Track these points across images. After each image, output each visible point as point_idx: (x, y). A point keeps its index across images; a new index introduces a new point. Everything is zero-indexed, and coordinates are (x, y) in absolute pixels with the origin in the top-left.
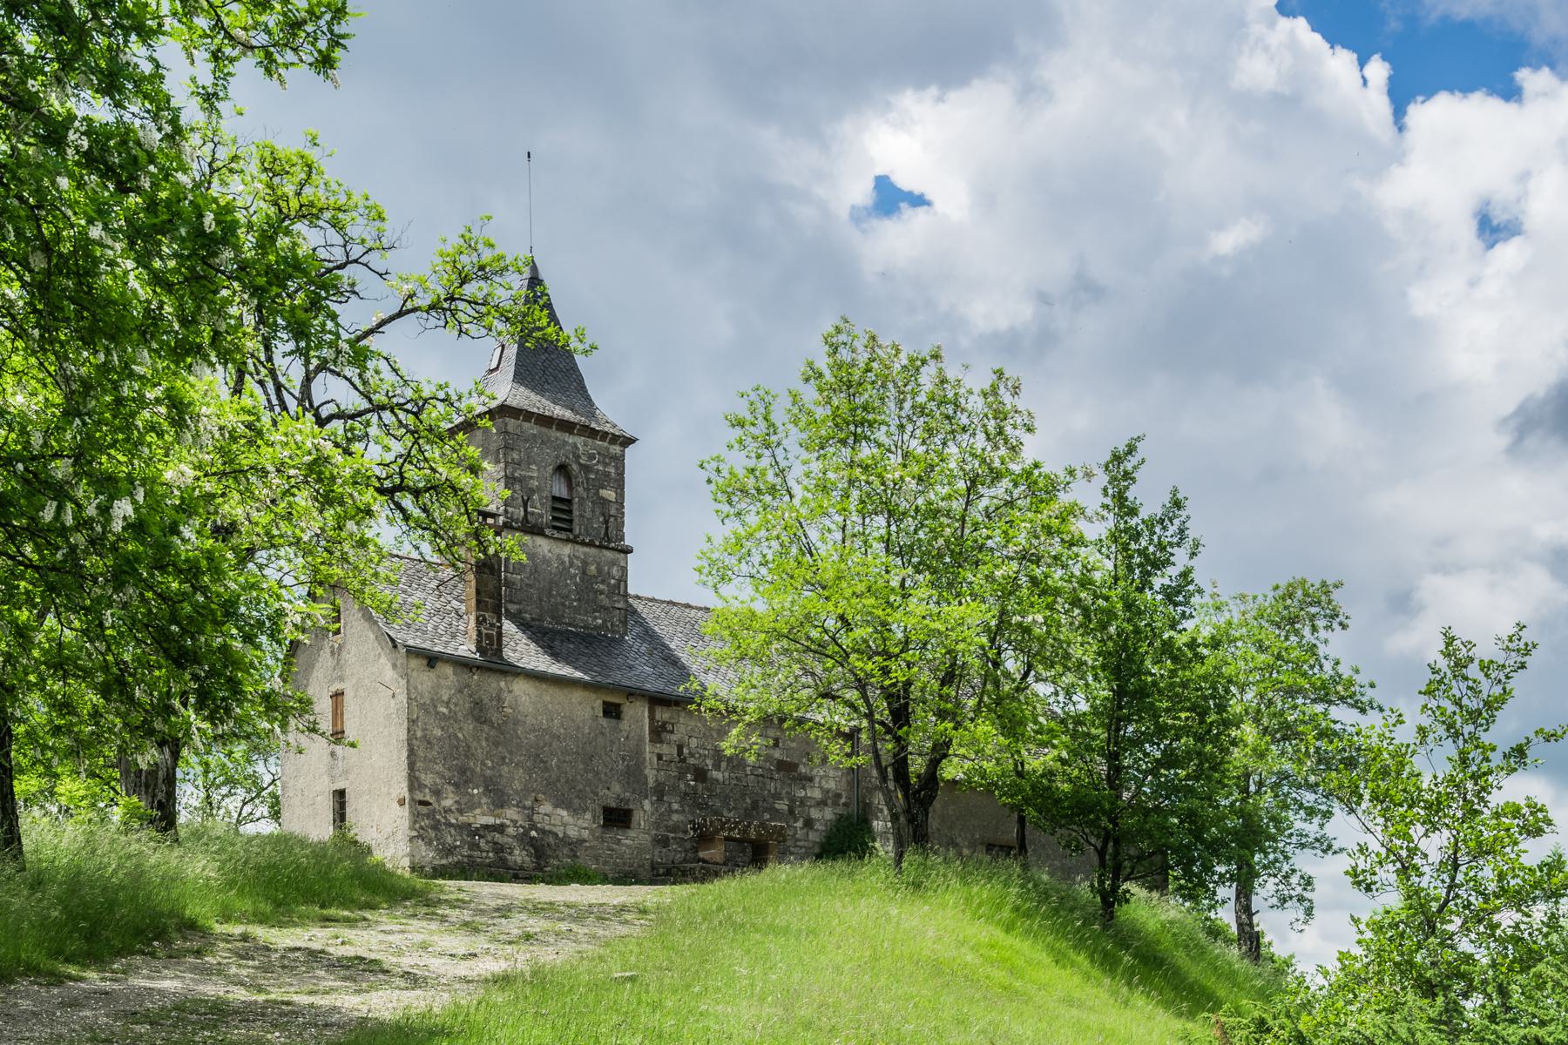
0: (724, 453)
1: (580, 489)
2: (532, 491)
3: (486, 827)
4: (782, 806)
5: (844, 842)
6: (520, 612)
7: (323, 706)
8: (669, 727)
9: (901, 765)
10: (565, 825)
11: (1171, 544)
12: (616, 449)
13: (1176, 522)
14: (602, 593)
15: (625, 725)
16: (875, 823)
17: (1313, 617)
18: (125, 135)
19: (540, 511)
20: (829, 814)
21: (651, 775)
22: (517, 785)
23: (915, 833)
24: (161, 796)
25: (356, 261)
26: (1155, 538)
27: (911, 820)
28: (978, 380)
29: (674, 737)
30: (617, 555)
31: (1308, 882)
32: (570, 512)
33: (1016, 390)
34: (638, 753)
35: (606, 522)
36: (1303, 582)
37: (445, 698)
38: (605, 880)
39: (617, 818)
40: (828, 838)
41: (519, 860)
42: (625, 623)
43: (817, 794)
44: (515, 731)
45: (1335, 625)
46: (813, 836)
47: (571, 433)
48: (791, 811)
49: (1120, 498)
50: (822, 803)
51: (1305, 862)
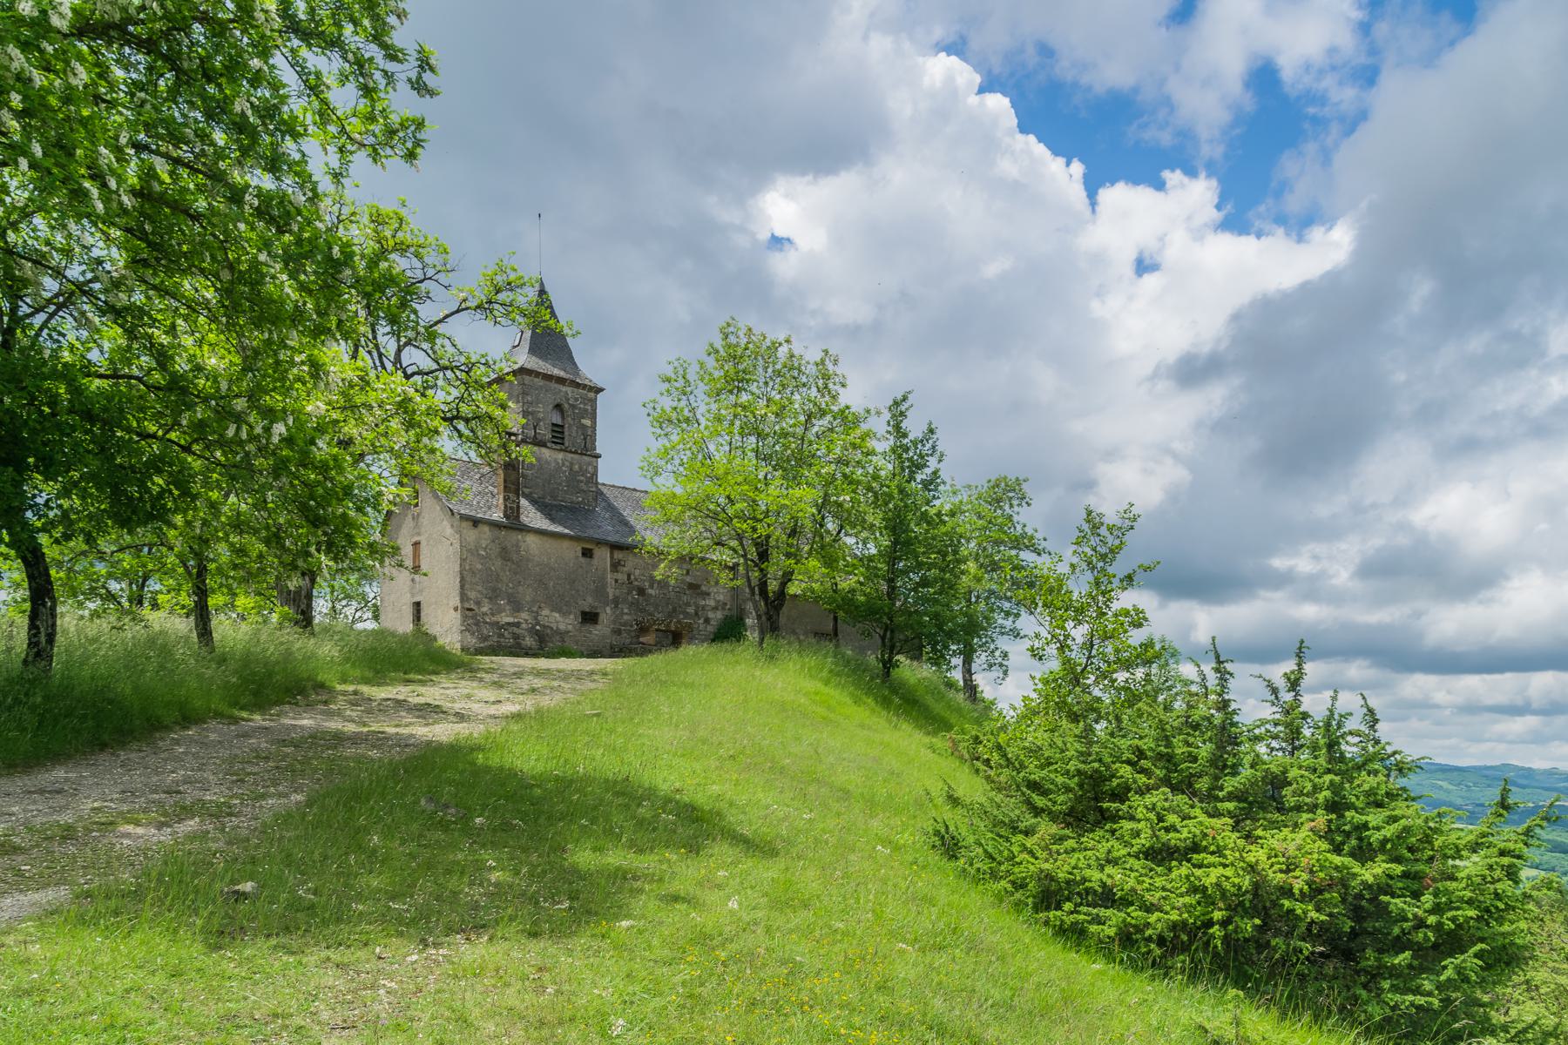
4: (691, 610)
5: (729, 631)
7: (407, 550)
9: (763, 585)
12: (591, 395)
15: (595, 561)
18: (283, 198)
19: (545, 432)
20: (719, 615)
21: (611, 592)
23: (771, 626)
31: (1005, 655)
33: (836, 362)
34: (603, 579)
39: (590, 618)
43: (712, 603)
49: (897, 427)
50: (715, 609)
51: (1003, 643)
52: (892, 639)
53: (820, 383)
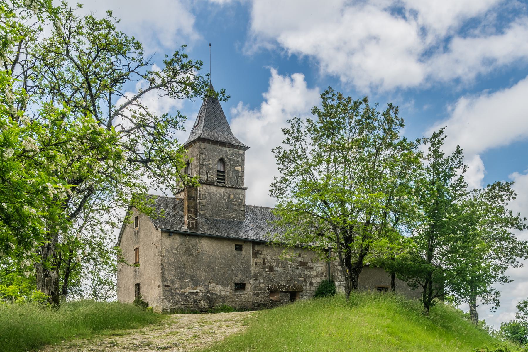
0: (282, 145)
1: (228, 167)
2: (210, 169)
3: (191, 293)
4: (301, 278)
5: (326, 290)
6: (205, 214)
8: (260, 252)
10: (220, 291)
11: (456, 168)
12: (241, 152)
13: (458, 159)
14: (235, 205)
15: (243, 252)
16: (336, 282)
17: (502, 196)
19: (213, 176)
20: (319, 280)
21: (253, 271)
22: (203, 277)
24: (52, 290)
25: (133, 71)
26: (449, 166)
27: (351, 280)
28: (382, 108)
29: (262, 256)
30: (241, 191)
31: (497, 293)
32: (224, 176)
33: (396, 112)
34: (248, 262)
35: (237, 179)
36: (499, 183)
37: (176, 247)
38: (235, 310)
40: (318, 289)
41: (203, 305)
42: (244, 215)
43: (315, 273)
44: (202, 258)
45: (511, 198)
46: (313, 289)
47: (225, 147)
48: (305, 280)
49: (435, 152)
50: (316, 276)
52: (430, 289)
53: (386, 127)
